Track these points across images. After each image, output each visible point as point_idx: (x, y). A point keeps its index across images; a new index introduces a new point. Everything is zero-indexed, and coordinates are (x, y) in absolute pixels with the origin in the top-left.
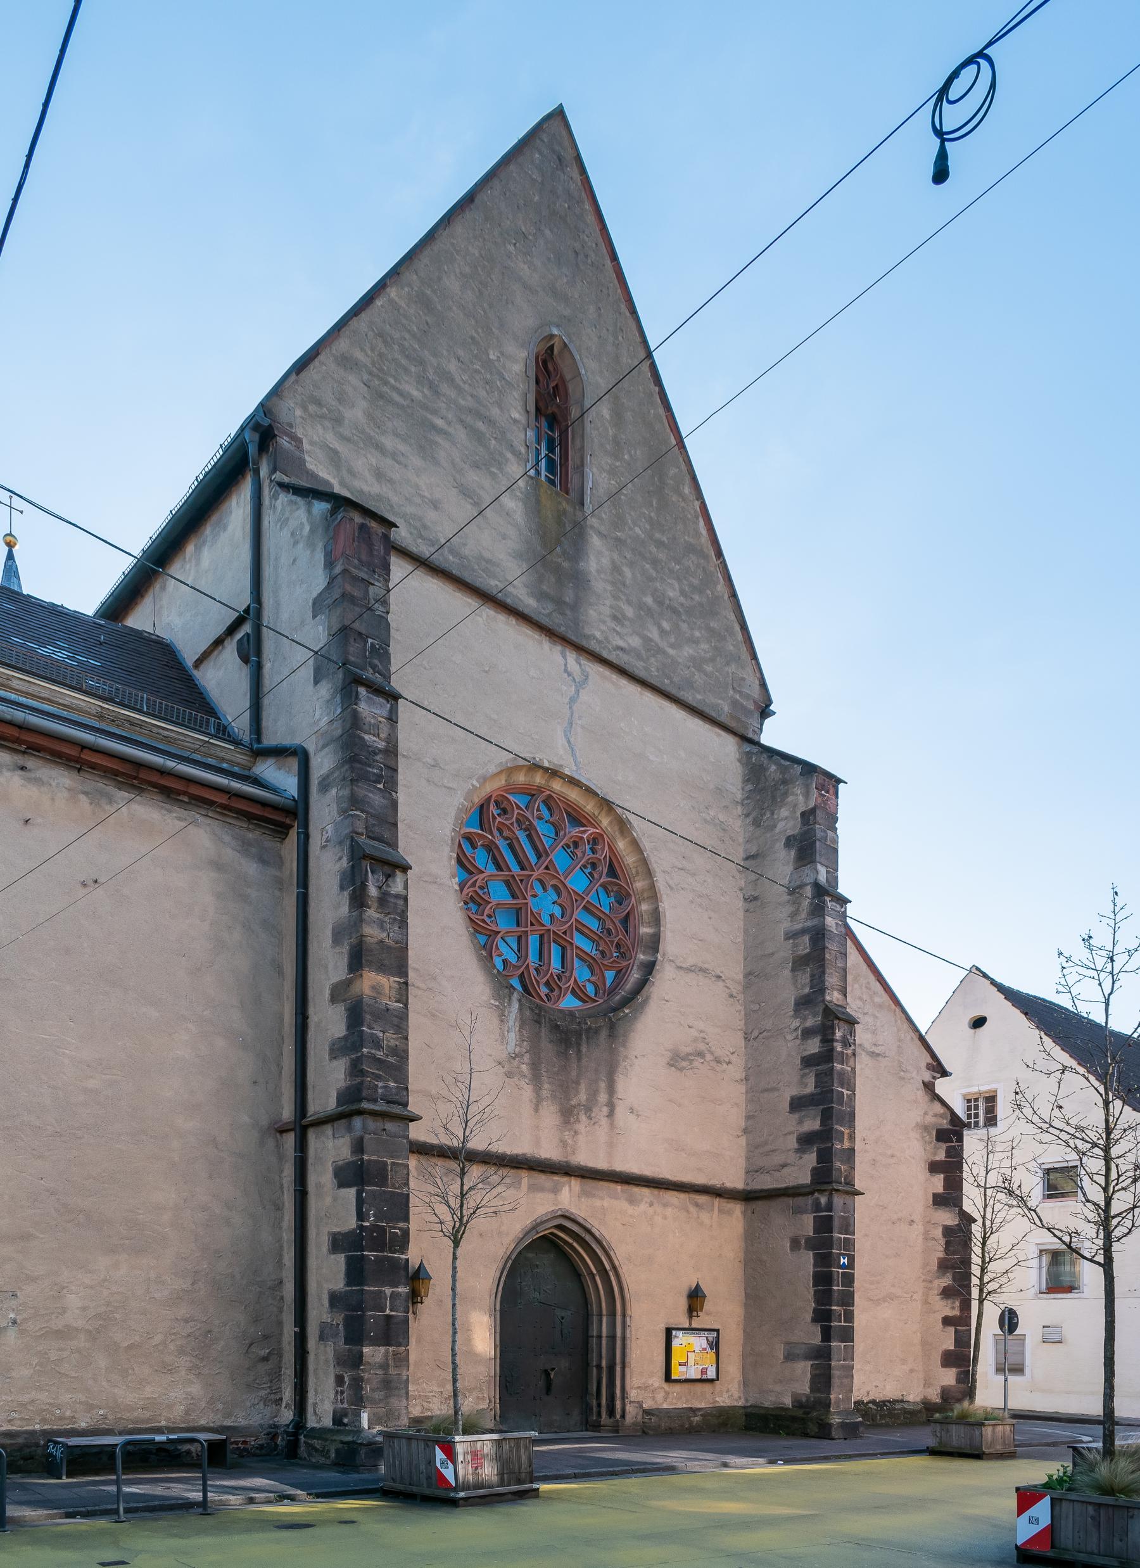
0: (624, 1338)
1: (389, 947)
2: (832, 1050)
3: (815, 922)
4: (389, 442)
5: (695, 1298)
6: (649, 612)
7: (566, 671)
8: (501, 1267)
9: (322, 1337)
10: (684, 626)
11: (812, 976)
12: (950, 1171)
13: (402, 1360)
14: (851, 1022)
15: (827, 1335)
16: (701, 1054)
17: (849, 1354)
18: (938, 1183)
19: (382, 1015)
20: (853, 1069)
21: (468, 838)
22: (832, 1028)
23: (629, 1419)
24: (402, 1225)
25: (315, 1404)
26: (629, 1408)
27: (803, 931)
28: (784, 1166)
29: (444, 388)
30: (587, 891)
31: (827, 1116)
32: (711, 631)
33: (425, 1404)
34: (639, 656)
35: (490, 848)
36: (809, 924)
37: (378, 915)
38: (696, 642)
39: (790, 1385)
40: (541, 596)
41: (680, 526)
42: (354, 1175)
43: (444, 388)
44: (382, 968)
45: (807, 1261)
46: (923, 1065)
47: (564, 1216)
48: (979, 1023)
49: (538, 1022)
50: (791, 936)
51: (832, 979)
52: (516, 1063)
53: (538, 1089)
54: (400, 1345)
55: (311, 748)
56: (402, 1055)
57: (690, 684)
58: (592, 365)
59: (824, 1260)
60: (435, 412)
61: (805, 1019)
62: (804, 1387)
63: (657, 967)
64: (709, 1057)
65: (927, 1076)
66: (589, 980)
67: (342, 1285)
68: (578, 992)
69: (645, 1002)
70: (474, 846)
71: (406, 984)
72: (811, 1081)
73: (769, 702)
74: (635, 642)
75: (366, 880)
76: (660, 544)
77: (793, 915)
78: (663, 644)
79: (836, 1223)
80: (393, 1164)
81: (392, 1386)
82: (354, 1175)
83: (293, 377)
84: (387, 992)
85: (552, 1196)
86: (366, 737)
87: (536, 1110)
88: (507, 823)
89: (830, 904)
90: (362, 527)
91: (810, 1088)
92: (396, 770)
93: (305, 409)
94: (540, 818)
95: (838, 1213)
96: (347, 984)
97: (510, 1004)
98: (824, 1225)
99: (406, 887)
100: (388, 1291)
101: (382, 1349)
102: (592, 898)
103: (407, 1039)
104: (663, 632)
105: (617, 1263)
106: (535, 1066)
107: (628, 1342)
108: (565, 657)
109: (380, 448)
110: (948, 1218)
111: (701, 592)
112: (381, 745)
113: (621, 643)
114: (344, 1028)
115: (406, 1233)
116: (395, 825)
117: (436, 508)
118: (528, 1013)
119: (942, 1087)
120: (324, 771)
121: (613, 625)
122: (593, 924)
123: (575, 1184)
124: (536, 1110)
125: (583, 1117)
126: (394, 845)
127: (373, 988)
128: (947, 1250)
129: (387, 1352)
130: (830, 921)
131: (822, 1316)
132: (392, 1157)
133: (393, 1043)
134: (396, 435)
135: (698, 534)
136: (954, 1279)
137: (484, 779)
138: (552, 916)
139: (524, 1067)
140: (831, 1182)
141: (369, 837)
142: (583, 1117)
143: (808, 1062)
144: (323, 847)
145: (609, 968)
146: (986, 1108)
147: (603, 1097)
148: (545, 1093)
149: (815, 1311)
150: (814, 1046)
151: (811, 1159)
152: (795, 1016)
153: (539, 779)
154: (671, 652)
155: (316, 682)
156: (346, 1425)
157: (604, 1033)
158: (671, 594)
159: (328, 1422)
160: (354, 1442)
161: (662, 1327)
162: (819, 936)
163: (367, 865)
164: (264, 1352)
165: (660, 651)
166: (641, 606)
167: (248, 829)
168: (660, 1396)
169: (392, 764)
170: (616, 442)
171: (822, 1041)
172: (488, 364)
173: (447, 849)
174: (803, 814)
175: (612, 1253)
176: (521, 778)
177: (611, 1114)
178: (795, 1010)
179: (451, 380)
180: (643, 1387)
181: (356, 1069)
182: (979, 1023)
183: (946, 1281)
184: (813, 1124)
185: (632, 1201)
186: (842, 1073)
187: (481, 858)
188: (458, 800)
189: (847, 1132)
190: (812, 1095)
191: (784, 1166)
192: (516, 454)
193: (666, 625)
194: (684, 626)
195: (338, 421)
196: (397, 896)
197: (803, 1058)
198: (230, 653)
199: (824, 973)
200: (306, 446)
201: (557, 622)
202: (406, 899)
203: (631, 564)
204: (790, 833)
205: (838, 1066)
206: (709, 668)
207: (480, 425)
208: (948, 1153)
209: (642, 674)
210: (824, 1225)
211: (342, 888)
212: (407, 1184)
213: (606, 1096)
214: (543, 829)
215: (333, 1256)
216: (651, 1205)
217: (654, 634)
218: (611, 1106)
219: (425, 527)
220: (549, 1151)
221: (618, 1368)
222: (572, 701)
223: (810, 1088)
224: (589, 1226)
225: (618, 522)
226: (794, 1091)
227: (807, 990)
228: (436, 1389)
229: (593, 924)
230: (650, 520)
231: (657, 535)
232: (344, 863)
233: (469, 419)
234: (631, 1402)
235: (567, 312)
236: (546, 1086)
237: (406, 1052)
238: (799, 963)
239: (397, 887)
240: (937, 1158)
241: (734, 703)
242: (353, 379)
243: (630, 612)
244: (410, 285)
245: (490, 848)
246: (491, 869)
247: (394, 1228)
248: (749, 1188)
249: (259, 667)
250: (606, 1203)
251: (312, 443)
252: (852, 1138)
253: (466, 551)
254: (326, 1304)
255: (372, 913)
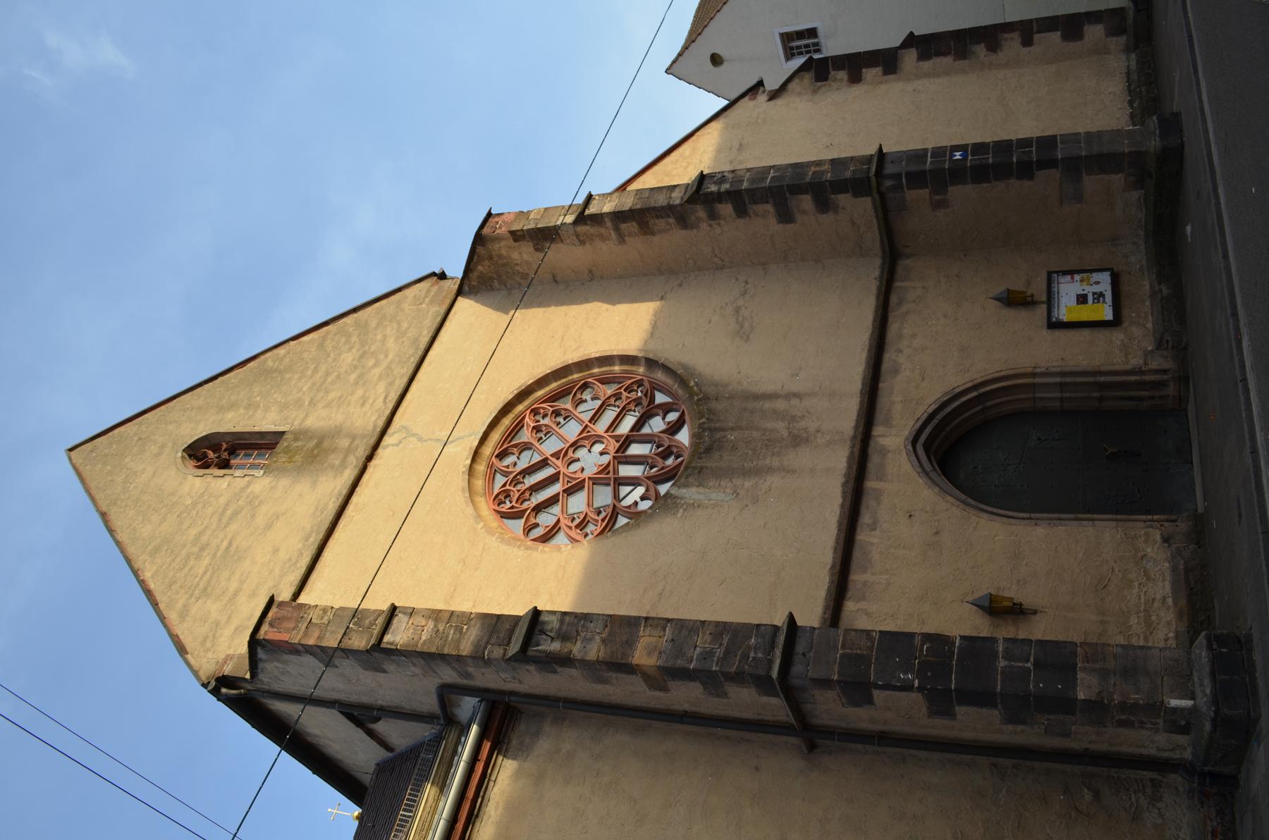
0: (1063, 374)
1: (610, 634)
2: (728, 192)
3: (607, 220)
4: (234, 585)
5: (1014, 300)
6: (360, 376)
7: (397, 445)
8: (975, 512)
9: (1067, 735)
10: (373, 348)
11: (658, 217)
12: (855, 66)
13: (1095, 652)
14: (702, 178)
15: (1051, 163)
16: (737, 310)
17: (1073, 138)
18: (870, 73)
19: (678, 647)
20: (748, 170)
21: (528, 530)
22: (706, 194)
23: (1166, 366)
24: (917, 640)
25: (1158, 749)
26: (1154, 365)
27: (617, 229)
28: (853, 222)
29: (204, 539)
30: (580, 421)
31: (797, 189)
32: (379, 324)
33: (1156, 605)
34: (391, 384)
35: (538, 509)
36: (609, 224)
37: (579, 643)
38: (385, 337)
39: (1119, 201)
40: (343, 465)
41: (305, 355)
42: (857, 689)
43: (204, 539)
44: (630, 643)
45: (957, 192)
46: (752, 103)
47: (914, 442)
48: (716, 60)
49: (701, 470)
50: (621, 238)
51: (661, 200)
52: (742, 492)
53: (770, 470)
54: (1074, 654)
55: (438, 681)
56: (721, 629)
57: (416, 340)
58: (201, 426)
59: (957, 174)
60: (218, 547)
61: (699, 219)
62: (1117, 179)
63: (651, 356)
64: (740, 302)
65: (762, 98)
66: (664, 419)
67: (996, 712)
68: (674, 428)
69: (684, 366)
70: (536, 525)
71: (647, 619)
72: (761, 208)
73: (434, 274)
74: (381, 388)
75: (545, 652)
76: (316, 370)
77: (603, 238)
78: (385, 364)
79: (914, 168)
80: (843, 647)
81: (1131, 664)
82: (857, 689)
83: (189, 657)
84: (654, 639)
85: (890, 455)
86: (424, 638)
87: (793, 472)
88: (517, 495)
89: (592, 210)
90: (271, 625)
91: (769, 207)
92: (453, 613)
93: (207, 651)
94: (515, 464)
95: (903, 167)
96: (647, 677)
97: (682, 498)
98: (917, 180)
99: (554, 613)
100: (1002, 663)
101: (1080, 675)
102: (586, 417)
103: (704, 622)
104: (375, 365)
105: (970, 385)
106: (746, 473)
107: (1067, 369)
108: (388, 446)
109: (236, 594)
110: (909, 59)
111: (350, 336)
112: (431, 624)
113: (381, 399)
114: (693, 684)
115: (927, 637)
116: (499, 617)
117: (277, 550)
118: (691, 480)
119: (772, 84)
120: (454, 674)
121: (367, 406)
122: (610, 415)
123: (878, 430)
124: (793, 472)
125: (802, 424)
126: (516, 619)
127: (649, 654)
128: (945, 54)
129: (1083, 669)
130: (608, 208)
131: (1026, 170)
132: (836, 648)
133: (708, 638)
134: (229, 579)
135: (312, 341)
136: (978, 43)
137: (479, 516)
138: (602, 454)
139: (747, 484)
140: (869, 178)
141: (508, 644)
142: (802, 424)
143: (741, 212)
144: (520, 682)
145: (652, 399)
146: (795, 41)
147: (780, 405)
148: (776, 462)
149: (1019, 178)
150: (726, 209)
151: (844, 199)
152: (698, 227)
153: (481, 468)
154: (391, 356)
155: (385, 671)
156: (1188, 723)
157: (713, 405)
158: (350, 359)
159: (1182, 739)
160: (1214, 720)
161: (1045, 333)
162: (619, 217)
163: (532, 651)
164: (1088, 796)
165: (389, 367)
166: (356, 383)
167: (508, 743)
168: (1136, 331)
169: (447, 616)
170: (248, 407)
171: (720, 202)
172: (194, 504)
173: (535, 554)
174: (515, 240)
175: (957, 391)
176: (479, 483)
177: (797, 395)
178: (692, 228)
179: (201, 533)
180: (1128, 351)
181: (738, 678)
182: (716, 60)
183: (980, 50)
184: (807, 201)
185: (896, 371)
186: (752, 181)
187: (546, 519)
188: (493, 541)
189: (813, 169)
190: (775, 205)
191: (853, 222)
192: (249, 483)
193: (371, 363)
194: (373, 348)
195: (217, 624)
196: (562, 622)
197: (739, 217)
198: (381, 727)
199: (654, 208)
200: (231, 652)
201: (362, 452)
202: (564, 614)
203: (327, 392)
204: (532, 249)
205: (745, 185)
206: (405, 325)
207: (229, 513)
208: (837, 68)
209: (405, 380)
210: (917, 180)
211: (555, 672)
212: (868, 632)
213: (779, 401)
214: (525, 460)
215: (959, 717)
216: (900, 351)
217: (377, 371)
218: (789, 396)
219: (290, 560)
220: (839, 460)
221: (1102, 379)
222: (420, 439)
223: (769, 207)
224: (926, 415)
225: (298, 403)
226: (773, 221)
227: (671, 220)
228: (1135, 591)
229: (610, 415)
230: (300, 379)
231: (309, 373)
232: (532, 668)
233: (225, 520)
234: (1146, 364)
235: (170, 445)
236: (768, 461)
237: (718, 623)
238: (645, 229)
239: (554, 623)
240: (846, 77)
241: (432, 302)
242: (193, 611)
243: (360, 392)
244: (145, 562)
245: (538, 509)
246: (556, 509)
247: (922, 650)
248: (880, 253)
249: (381, 709)
250: (898, 398)
251: (230, 647)
252: (818, 163)
253: (308, 527)
254: (1020, 728)
255: (576, 649)
